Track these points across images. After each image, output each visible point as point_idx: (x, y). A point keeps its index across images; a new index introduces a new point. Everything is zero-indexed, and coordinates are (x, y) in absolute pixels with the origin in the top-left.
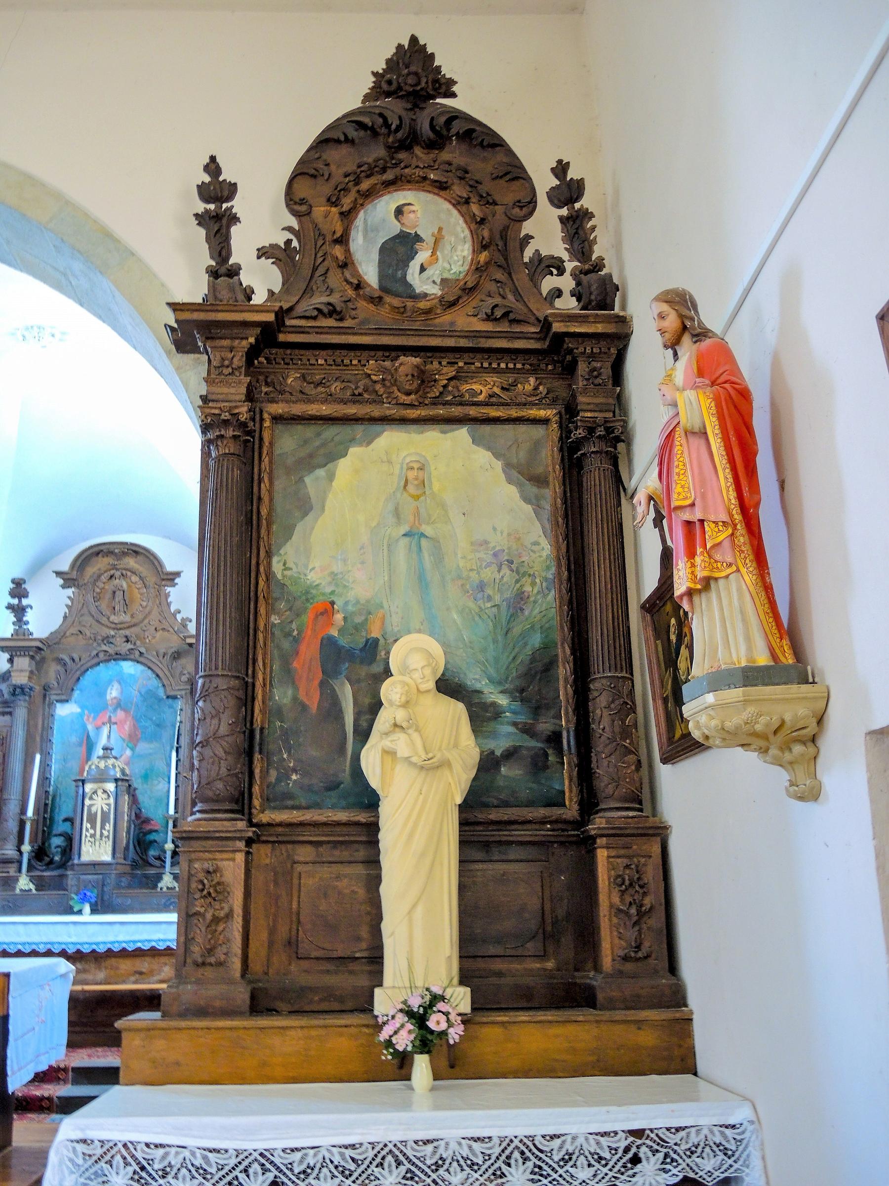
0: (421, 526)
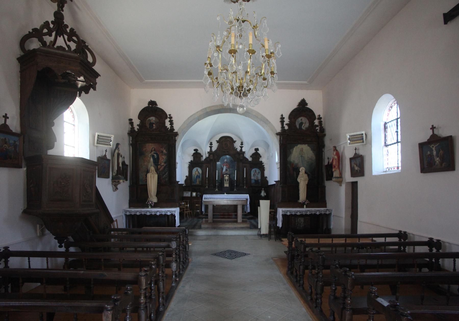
0: (302, 153)
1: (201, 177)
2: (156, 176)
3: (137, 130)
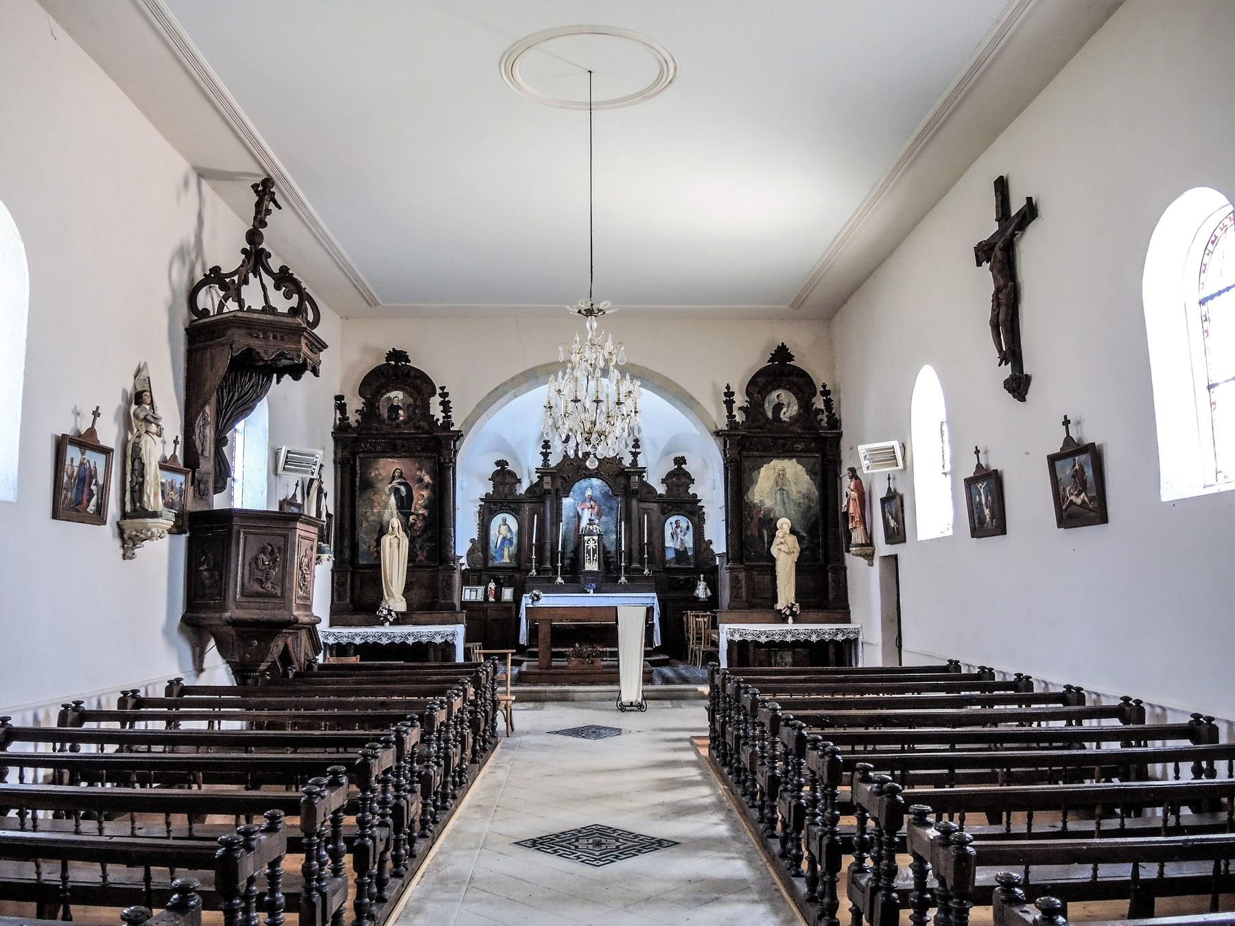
0: (781, 483)
1: (515, 541)
2: (405, 542)
3: (354, 424)
